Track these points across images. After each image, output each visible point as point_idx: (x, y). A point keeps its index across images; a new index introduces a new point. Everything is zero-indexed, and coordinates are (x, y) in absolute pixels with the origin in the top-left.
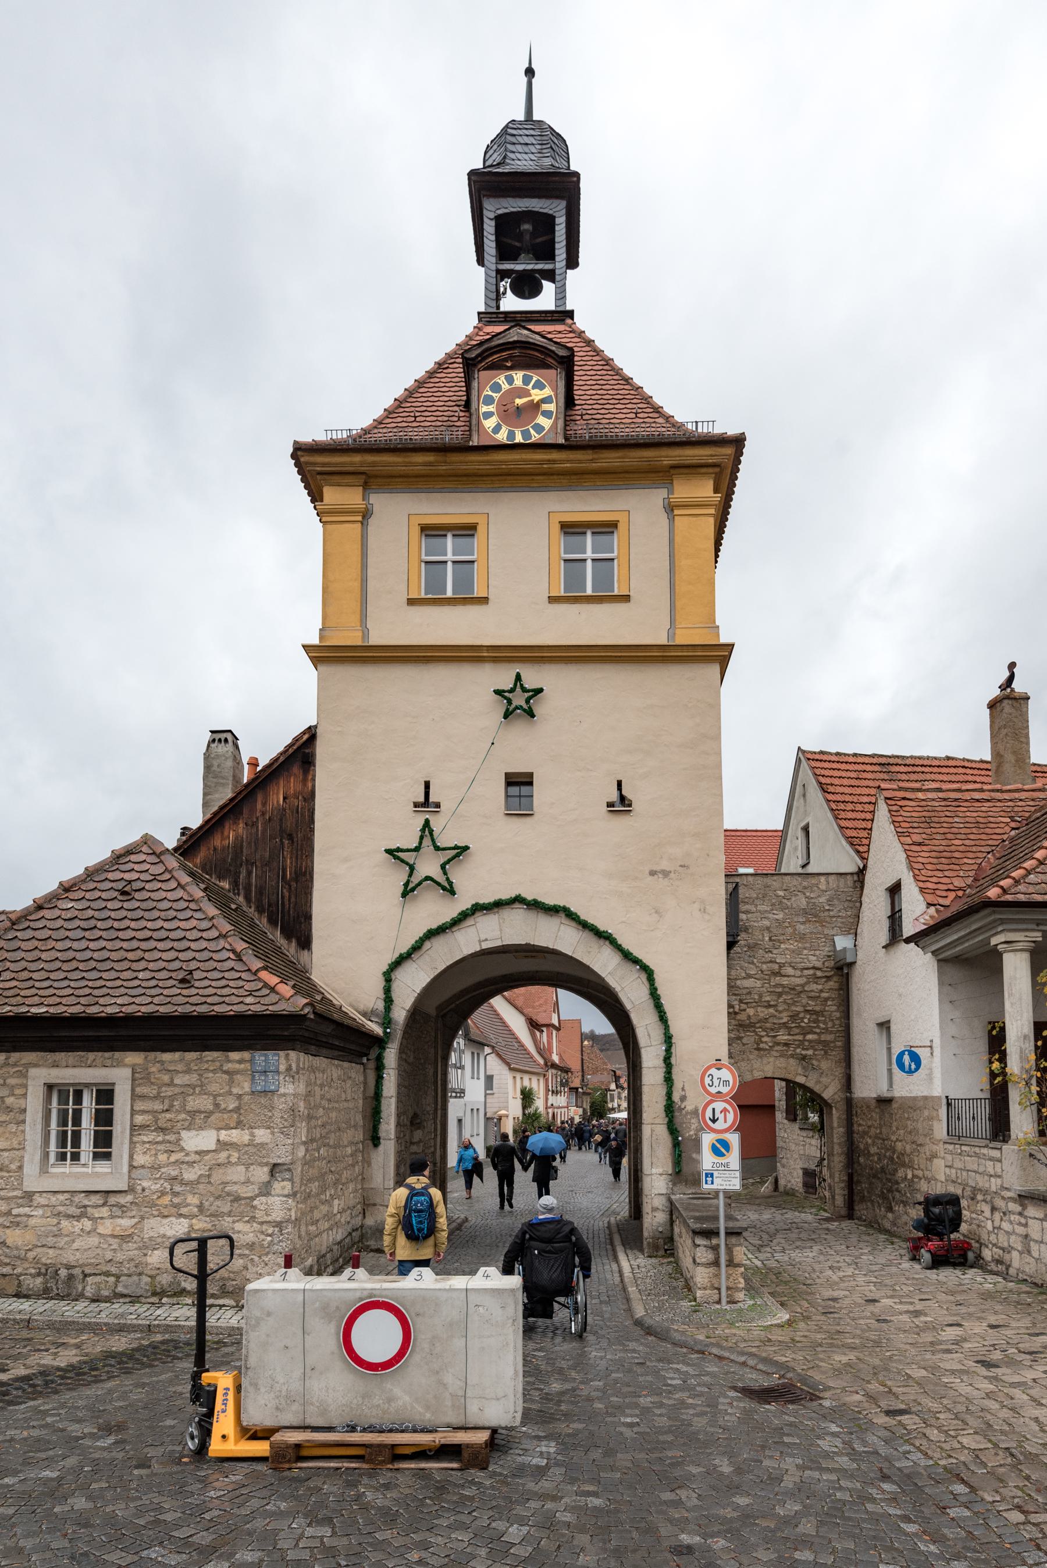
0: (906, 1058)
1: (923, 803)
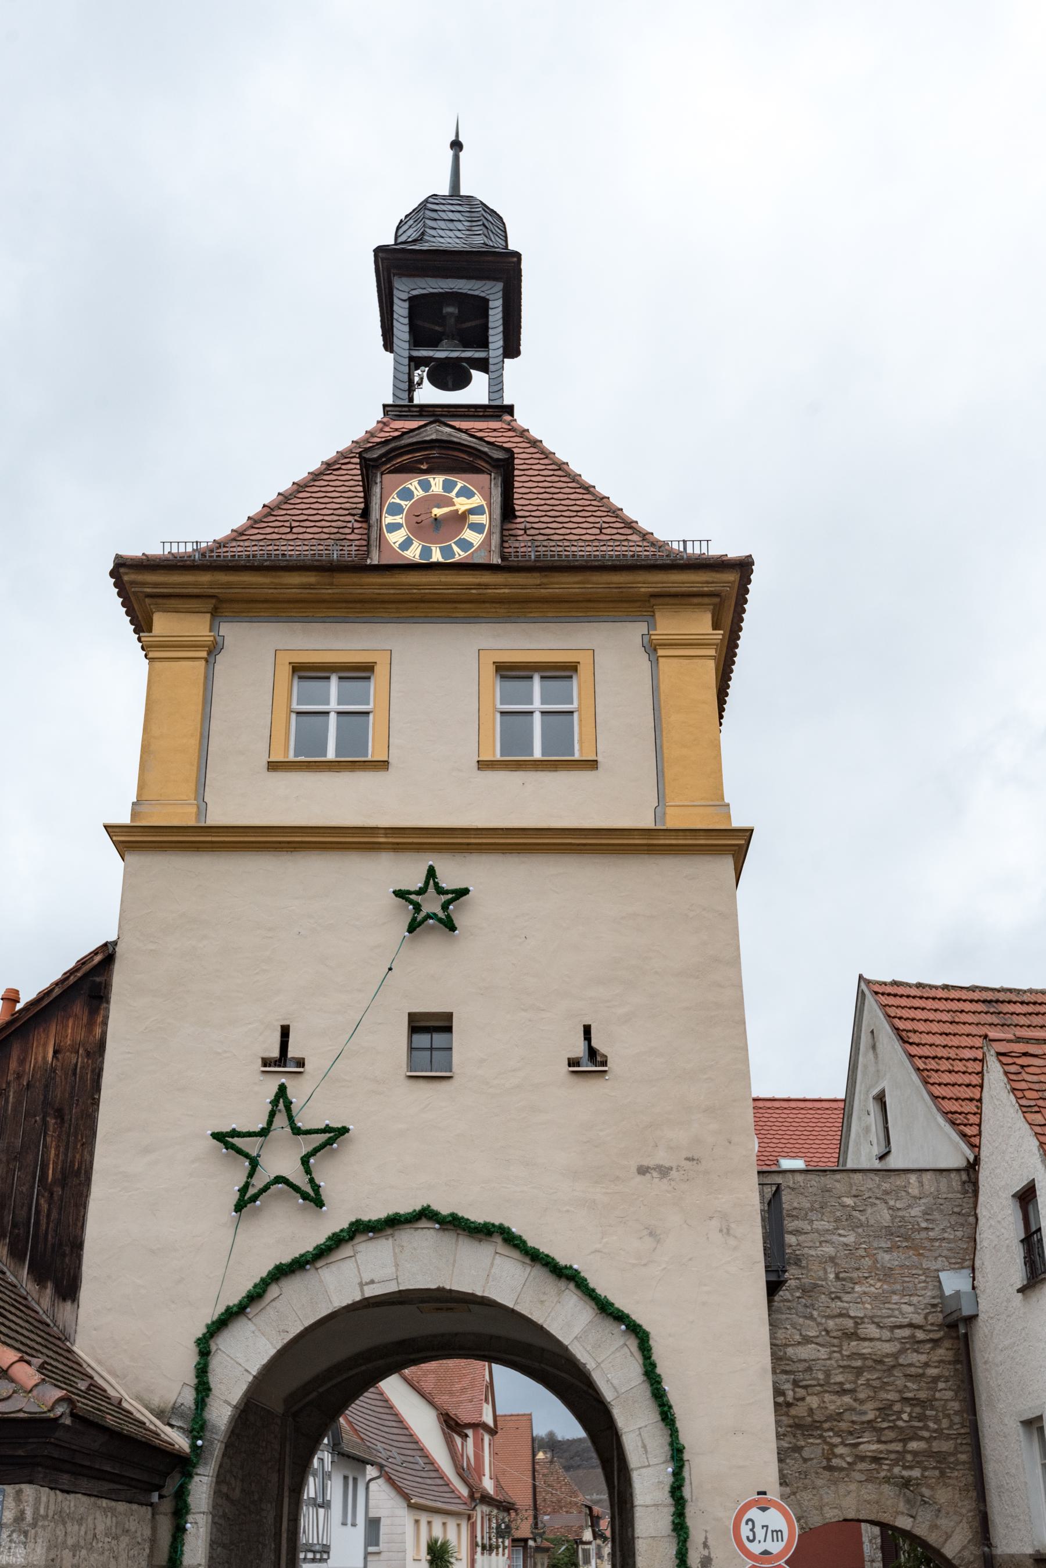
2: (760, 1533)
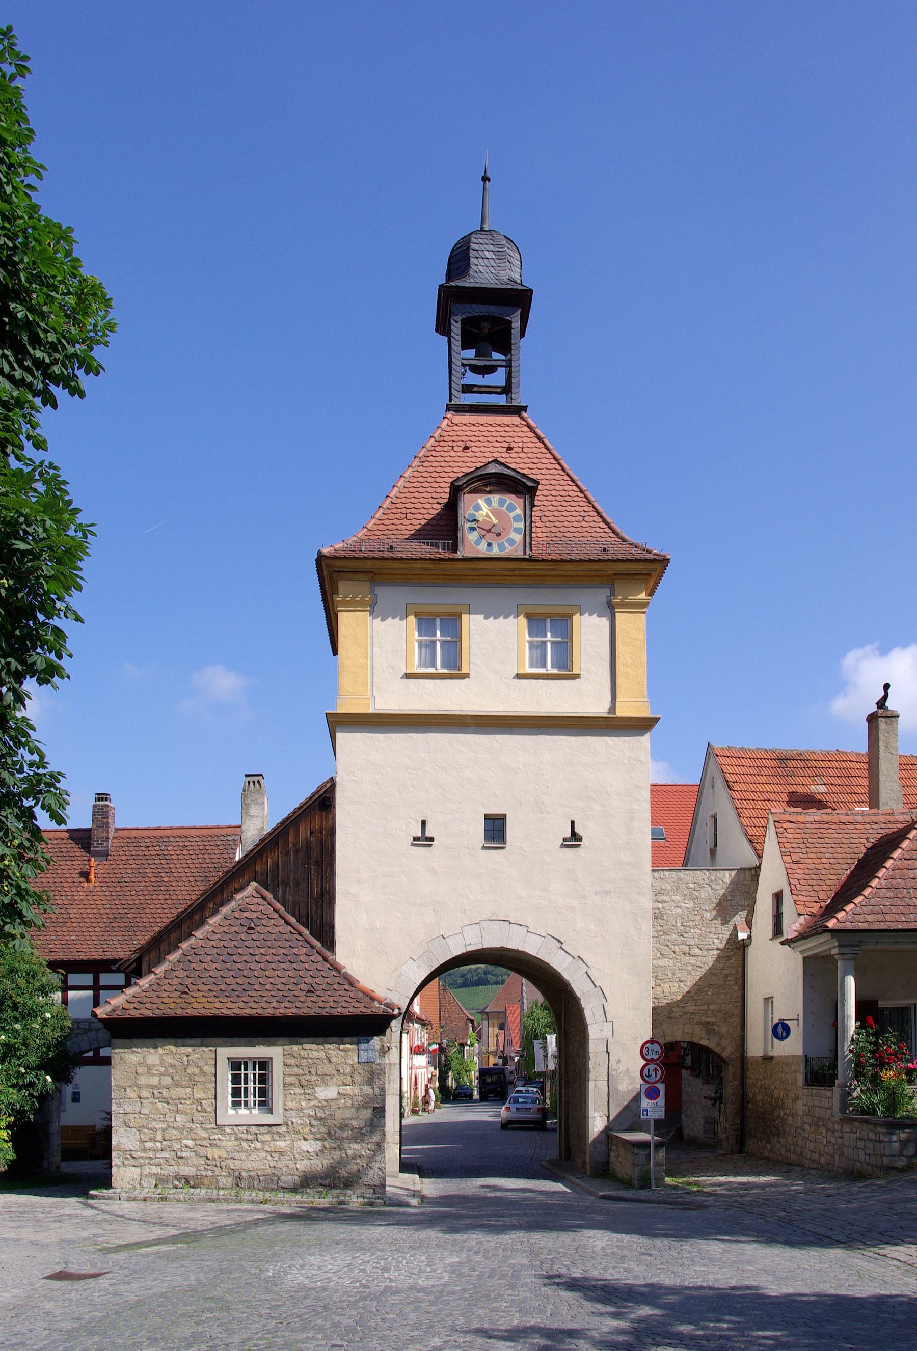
0: (780, 1028)
1: (801, 826)
2: (650, 1052)
